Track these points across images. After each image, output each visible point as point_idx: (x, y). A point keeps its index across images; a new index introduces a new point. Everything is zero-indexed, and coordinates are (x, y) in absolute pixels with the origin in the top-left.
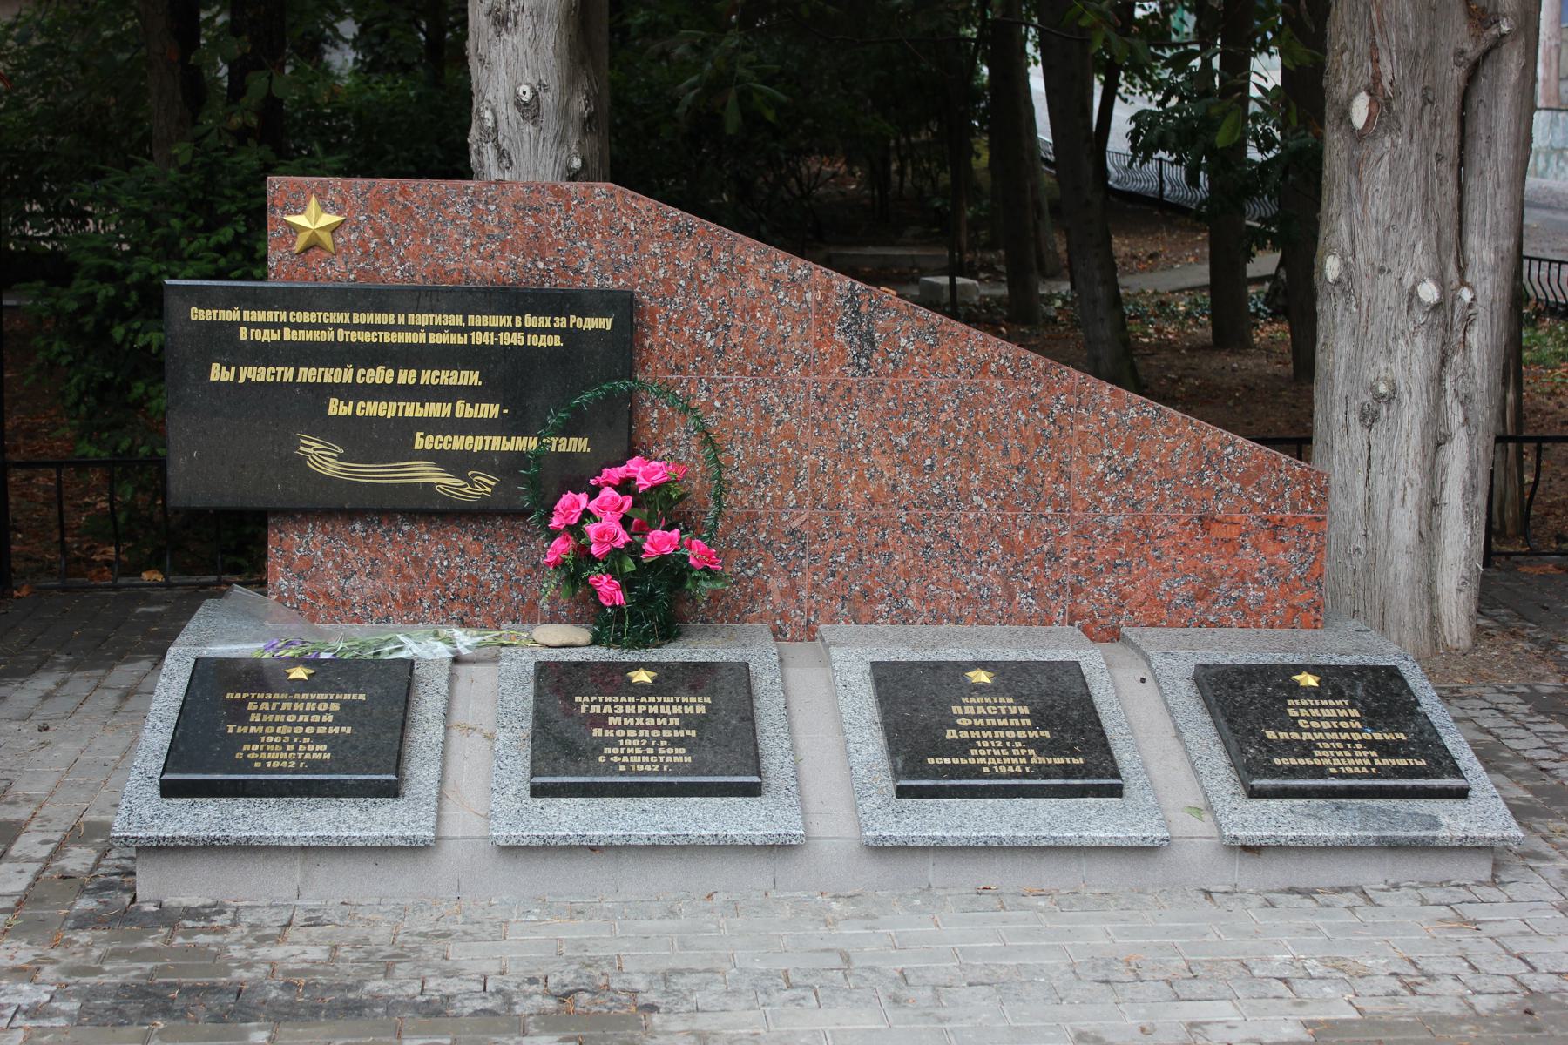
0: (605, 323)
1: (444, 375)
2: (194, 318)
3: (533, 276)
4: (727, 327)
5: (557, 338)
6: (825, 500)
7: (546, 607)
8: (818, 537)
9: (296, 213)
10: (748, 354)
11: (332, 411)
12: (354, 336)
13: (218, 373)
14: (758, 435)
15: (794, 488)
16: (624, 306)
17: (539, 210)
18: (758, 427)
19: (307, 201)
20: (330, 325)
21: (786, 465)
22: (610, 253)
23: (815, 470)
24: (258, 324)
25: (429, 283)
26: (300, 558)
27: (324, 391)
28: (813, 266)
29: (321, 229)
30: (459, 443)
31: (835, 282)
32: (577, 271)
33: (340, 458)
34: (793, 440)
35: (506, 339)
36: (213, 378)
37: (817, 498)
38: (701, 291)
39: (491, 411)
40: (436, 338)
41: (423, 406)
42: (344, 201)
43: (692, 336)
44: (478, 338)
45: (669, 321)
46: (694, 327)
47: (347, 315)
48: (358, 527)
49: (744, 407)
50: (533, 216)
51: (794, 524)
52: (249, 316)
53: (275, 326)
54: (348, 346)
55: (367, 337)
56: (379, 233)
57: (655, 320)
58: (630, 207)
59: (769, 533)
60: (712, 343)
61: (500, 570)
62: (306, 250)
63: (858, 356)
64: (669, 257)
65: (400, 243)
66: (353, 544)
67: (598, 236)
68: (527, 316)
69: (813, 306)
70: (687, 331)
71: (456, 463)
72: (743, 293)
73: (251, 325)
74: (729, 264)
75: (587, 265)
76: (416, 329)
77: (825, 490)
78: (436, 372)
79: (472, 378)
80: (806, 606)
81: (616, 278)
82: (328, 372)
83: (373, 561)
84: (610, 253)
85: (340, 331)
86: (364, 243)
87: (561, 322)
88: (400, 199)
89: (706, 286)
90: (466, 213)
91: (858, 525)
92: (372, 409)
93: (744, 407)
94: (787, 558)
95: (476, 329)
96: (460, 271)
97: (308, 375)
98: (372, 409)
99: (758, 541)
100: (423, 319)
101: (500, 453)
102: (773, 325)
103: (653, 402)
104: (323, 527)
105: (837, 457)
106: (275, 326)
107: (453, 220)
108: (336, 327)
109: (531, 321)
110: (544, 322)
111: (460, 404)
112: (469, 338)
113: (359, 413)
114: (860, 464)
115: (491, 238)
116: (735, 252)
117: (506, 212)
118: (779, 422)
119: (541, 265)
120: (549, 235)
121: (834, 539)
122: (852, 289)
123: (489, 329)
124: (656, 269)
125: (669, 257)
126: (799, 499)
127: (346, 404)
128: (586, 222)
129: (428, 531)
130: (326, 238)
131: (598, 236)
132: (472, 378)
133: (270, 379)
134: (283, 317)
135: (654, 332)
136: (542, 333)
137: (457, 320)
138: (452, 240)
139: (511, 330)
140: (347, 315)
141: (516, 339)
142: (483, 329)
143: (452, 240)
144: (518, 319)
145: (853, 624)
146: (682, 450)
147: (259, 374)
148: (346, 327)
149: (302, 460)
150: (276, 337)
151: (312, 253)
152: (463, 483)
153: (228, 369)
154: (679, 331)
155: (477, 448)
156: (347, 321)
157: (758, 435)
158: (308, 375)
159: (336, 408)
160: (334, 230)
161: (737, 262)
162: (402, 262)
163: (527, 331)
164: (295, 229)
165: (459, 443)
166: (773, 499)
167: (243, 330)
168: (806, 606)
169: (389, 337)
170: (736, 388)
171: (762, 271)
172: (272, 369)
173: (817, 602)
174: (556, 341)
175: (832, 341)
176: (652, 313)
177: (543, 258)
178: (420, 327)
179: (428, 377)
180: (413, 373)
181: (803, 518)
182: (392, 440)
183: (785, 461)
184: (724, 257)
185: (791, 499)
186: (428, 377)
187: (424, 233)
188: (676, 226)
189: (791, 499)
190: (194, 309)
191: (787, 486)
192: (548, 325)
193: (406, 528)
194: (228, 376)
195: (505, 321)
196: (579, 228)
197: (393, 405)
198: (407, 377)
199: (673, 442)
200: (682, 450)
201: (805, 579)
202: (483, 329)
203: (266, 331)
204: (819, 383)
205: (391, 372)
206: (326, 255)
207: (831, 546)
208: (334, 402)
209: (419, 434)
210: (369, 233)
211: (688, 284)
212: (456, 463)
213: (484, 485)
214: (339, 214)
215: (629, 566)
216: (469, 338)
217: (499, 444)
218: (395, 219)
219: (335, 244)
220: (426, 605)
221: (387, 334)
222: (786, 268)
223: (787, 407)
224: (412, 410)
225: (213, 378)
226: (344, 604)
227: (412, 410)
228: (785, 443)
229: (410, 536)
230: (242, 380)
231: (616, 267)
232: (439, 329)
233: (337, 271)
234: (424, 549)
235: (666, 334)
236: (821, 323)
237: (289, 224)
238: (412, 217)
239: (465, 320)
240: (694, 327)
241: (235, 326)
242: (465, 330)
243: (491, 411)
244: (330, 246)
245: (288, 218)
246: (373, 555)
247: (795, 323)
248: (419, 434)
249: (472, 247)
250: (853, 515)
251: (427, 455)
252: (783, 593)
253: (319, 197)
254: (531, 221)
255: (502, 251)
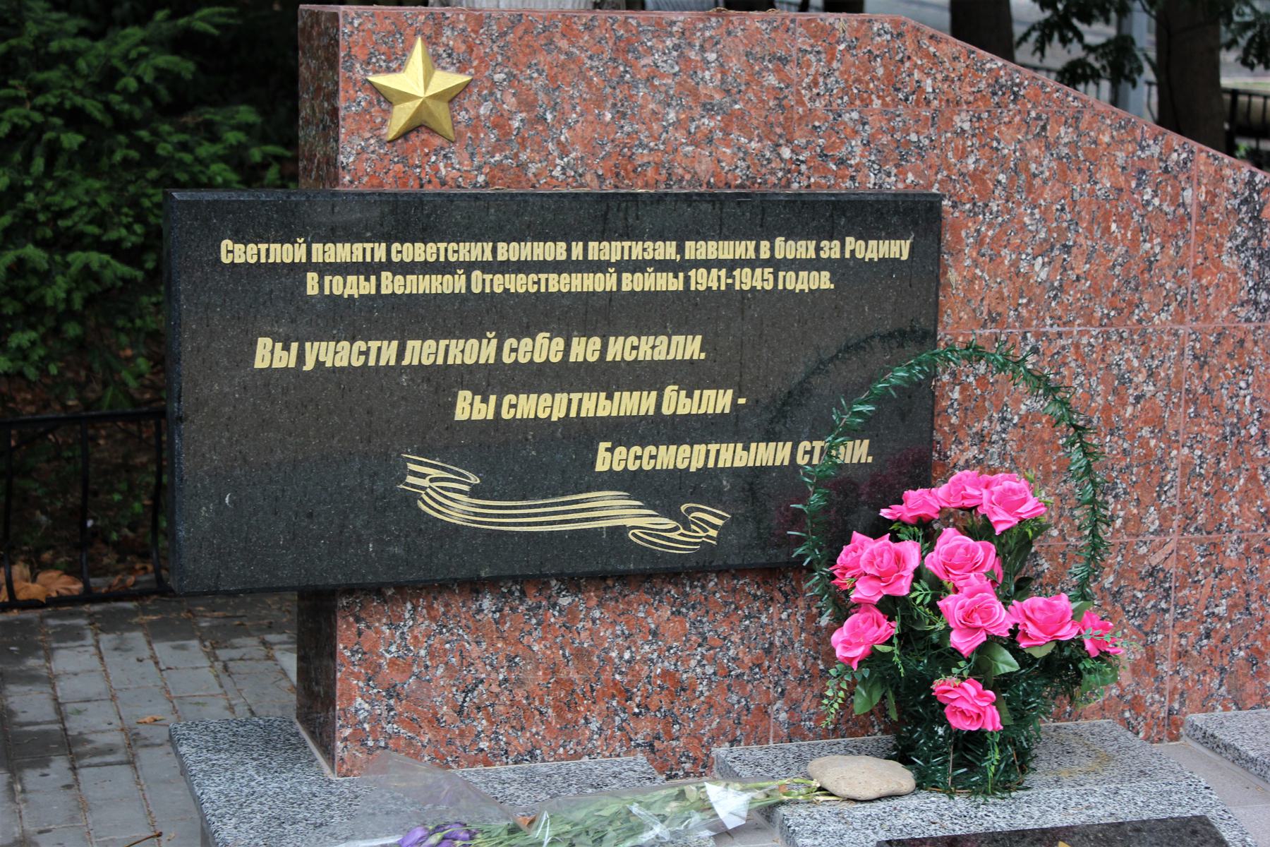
0: (899, 249)
1: (646, 343)
2: (226, 259)
3: (773, 173)
4: (1067, 249)
5: (826, 275)
6: (1201, 519)
7: (783, 716)
8: (1189, 577)
9: (389, 70)
10: (1096, 291)
11: (461, 413)
12: (500, 283)
13: (269, 355)
14: (1108, 421)
15: (1156, 502)
16: (918, 216)
17: (784, 60)
18: (1107, 408)
19: (408, 49)
20: (459, 264)
21: (1146, 466)
22: (893, 131)
23: (1189, 472)
24: (337, 266)
25: (608, 188)
26: (392, 663)
27: (447, 380)
28: (1196, 146)
29: (436, 97)
30: (669, 457)
31: (1227, 172)
32: (841, 162)
33: (475, 492)
34: (1158, 425)
35: (746, 280)
36: (259, 364)
37: (1190, 518)
38: (1029, 192)
39: (718, 401)
40: (632, 282)
41: (610, 397)
42: (470, 49)
43: (1015, 264)
44: (702, 280)
45: (980, 242)
46: (1019, 250)
47: (488, 247)
48: (487, 603)
49: (1088, 376)
50: (777, 71)
51: (1155, 560)
52: (321, 253)
53: (367, 269)
54: (488, 299)
55: (520, 283)
56: (527, 104)
57: (959, 240)
58: (927, 55)
59: (1119, 575)
60: (1043, 275)
61: (713, 661)
62: (404, 134)
63: (1256, 288)
64: (983, 134)
65: (562, 120)
66: (477, 631)
67: (877, 103)
68: (779, 241)
69: (1193, 210)
70: (1007, 256)
71: (658, 490)
72: (1092, 193)
73: (325, 269)
74: (1073, 145)
75: (858, 151)
76: (600, 267)
77: (1202, 505)
78: (633, 340)
79: (689, 347)
80: (1168, 686)
81: (901, 174)
82: (455, 346)
83: (511, 659)
84: (893, 131)
85: (477, 274)
86: (500, 122)
87: (831, 250)
88: (563, 44)
89: (1037, 182)
90: (668, 66)
91: (1246, 555)
92: (528, 406)
93: (1088, 376)
94: (1142, 614)
95: (697, 264)
96: (658, 166)
97: (422, 352)
98: (528, 406)
99: (1102, 589)
100: (612, 250)
101: (734, 472)
102: (1135, 243)
103: (953, 374)
104: (430, 608)
105: (1219, 450)
106: (367, 269)
107: (649, 80)
108: (469, 267)
109: (786, 248)
110: (804, 249)
111: (670, 391)
112: (687, 279)
113: (506, 415)
114: (1252, 459)
115: (709, 108)
116: (1083, 125)
117: (734, 65)
118: (1138, 399)
119: (786, 153)
120: (802, 103)
121: (1212, 580)
122: (1250, 183)
123: (719, 264)
124: (963, 155)
125: (983, 134)
126: (1164, 518)
127: (485, 400)
128: (858, 80)
129: (600, 605)
130: (442, 114)
131: (877, 103)
132: (689, 347)
133: (358, 362)
134: (380, 252)
135: (958, 261)
136: (798, 268)
137: (667, 250)
138: (646, 113)
139: (753, 264)
140: (488, 247)
141: (759, 280)
142: (708, 264)
143: (646, 113)
144: (765, 245)
145: (1233, 711)
146: (995, 449)
147: (339, 354)
148: (487, 267)
149: (410, 499)
150: (368, 288)
151: (414, 139)
152: (672, 524)
153: (286, 348)
154: (995, 259)
155: (697, 464)
156: (488, 256)
157: (1108, 421)
158: (422, 352)
159: (469, 407)
160: (452, 98)
161: (1085, 143)
162: (564, 153)
163: (777, 265)
164: (386, 99)
165: (669, 457)
166: (1126, 521)
167: (312, 278)
168: (1168, 686)
169: (557, 283)
170: (1077, 346)
171: (1121, 156)
172: (360, 345)
173: (1184, 680)
174: (823, 281)
175: (1218, 266)
176: (956, 229)
177: (789, 142)
178: (609, 264)
179: (619, 349)
180: (596, 342)
181: (1168, 549)
182: (560, 458)
183: (1145, 462)
184: (1066, 134)
185: (1152, 520)
186: (619, 349)
187: (600, 102)
188: (996, 86)
189: (1152, 520)
190: (226, 244)
191: (1146, 500)
192: (812, 254)
193: (565, 601)
194: (284, 359)
195: (742, 249)
196: (846, 91)
197: (562, 398)
198: (585, 349)
199: (981, 438)
200: (995, 449)
201: (1167, 643)
202: (708, 264)
203: (352, 279)
204: (1199, 335)
205: (559, 343)
206: (438, 142)
207: (1206, 590)
208: (464, 397)
209: (603, 446)
210: (510, 102)
211: (1010, 179)
212: (658, 490)
213: (708, 523)
214: (461, 71)
215: (1006, 663)
216: (687, 279)
217: (731, 456)
218: (553, 79)
219: (455, 123)
220: (594, 726)
221: (553, 277)
222: (1156, 150)
223: (1151, 374)
224: (594, 405)
225: (259, 364)
226: (462, 734)
227: (594, 405)
228: (1145, 432)
229: (571, 614)
230: (309, 365)
231: (902, 153)
232: (638, 266)
233: (457, 170)
234: (593, 634)
235: (976, 264)
236: (1205, 238)
237: (375, 89)
238: (582, 75)
239: (680, 250)
240: (1019, 250)
241: (297, 270)
242: (679, 267)
243: (718, 401)
244: (447, 126)
245: (374, 79)
246: (510, 650)
247: (1167, 237)
248: (603, 446)
249: (678, 124)
250: (1240, 540)
251: (615, 480)
252: (1135, 669)
253: (429, 41)
254: (772, 80)
255: (726, 131)
